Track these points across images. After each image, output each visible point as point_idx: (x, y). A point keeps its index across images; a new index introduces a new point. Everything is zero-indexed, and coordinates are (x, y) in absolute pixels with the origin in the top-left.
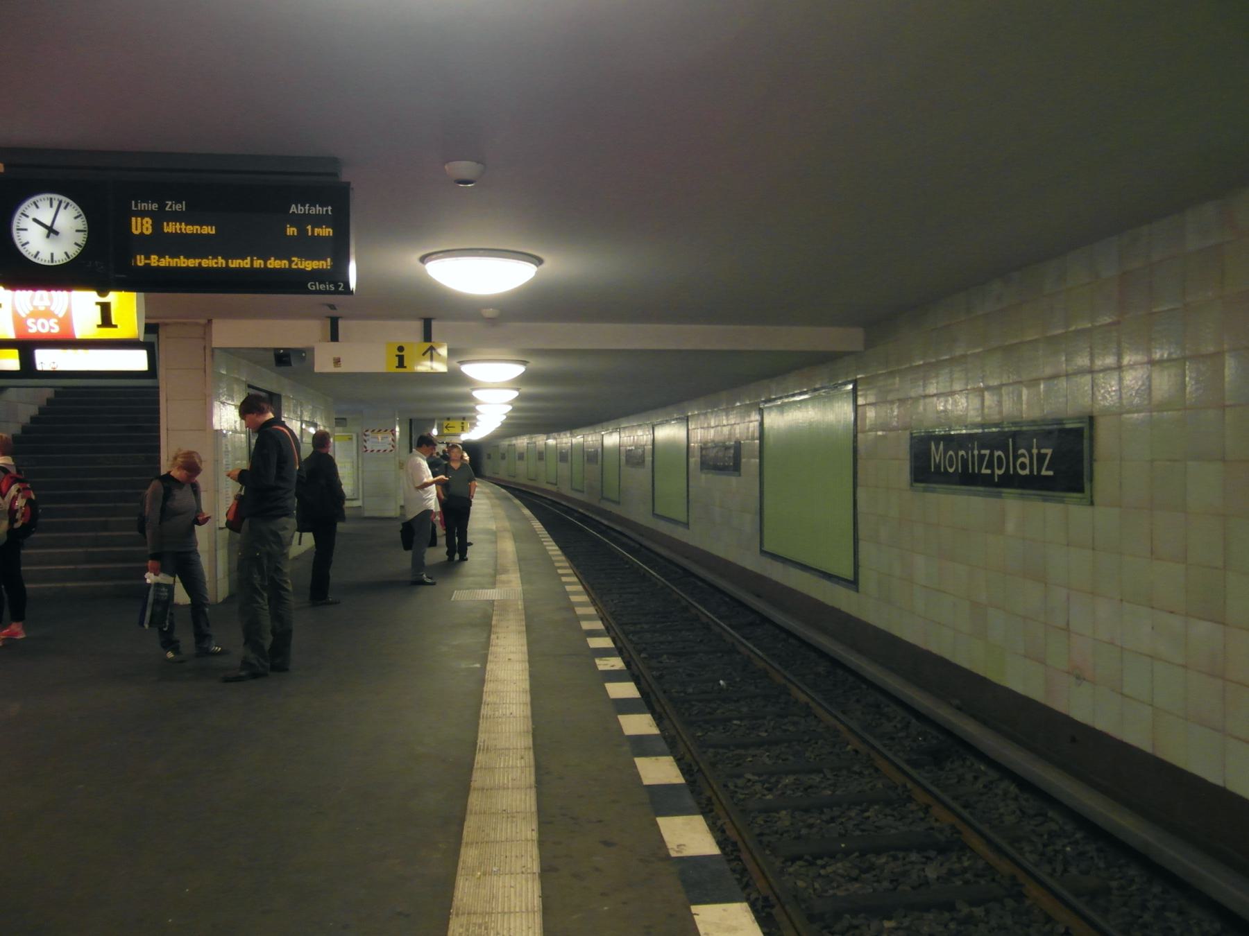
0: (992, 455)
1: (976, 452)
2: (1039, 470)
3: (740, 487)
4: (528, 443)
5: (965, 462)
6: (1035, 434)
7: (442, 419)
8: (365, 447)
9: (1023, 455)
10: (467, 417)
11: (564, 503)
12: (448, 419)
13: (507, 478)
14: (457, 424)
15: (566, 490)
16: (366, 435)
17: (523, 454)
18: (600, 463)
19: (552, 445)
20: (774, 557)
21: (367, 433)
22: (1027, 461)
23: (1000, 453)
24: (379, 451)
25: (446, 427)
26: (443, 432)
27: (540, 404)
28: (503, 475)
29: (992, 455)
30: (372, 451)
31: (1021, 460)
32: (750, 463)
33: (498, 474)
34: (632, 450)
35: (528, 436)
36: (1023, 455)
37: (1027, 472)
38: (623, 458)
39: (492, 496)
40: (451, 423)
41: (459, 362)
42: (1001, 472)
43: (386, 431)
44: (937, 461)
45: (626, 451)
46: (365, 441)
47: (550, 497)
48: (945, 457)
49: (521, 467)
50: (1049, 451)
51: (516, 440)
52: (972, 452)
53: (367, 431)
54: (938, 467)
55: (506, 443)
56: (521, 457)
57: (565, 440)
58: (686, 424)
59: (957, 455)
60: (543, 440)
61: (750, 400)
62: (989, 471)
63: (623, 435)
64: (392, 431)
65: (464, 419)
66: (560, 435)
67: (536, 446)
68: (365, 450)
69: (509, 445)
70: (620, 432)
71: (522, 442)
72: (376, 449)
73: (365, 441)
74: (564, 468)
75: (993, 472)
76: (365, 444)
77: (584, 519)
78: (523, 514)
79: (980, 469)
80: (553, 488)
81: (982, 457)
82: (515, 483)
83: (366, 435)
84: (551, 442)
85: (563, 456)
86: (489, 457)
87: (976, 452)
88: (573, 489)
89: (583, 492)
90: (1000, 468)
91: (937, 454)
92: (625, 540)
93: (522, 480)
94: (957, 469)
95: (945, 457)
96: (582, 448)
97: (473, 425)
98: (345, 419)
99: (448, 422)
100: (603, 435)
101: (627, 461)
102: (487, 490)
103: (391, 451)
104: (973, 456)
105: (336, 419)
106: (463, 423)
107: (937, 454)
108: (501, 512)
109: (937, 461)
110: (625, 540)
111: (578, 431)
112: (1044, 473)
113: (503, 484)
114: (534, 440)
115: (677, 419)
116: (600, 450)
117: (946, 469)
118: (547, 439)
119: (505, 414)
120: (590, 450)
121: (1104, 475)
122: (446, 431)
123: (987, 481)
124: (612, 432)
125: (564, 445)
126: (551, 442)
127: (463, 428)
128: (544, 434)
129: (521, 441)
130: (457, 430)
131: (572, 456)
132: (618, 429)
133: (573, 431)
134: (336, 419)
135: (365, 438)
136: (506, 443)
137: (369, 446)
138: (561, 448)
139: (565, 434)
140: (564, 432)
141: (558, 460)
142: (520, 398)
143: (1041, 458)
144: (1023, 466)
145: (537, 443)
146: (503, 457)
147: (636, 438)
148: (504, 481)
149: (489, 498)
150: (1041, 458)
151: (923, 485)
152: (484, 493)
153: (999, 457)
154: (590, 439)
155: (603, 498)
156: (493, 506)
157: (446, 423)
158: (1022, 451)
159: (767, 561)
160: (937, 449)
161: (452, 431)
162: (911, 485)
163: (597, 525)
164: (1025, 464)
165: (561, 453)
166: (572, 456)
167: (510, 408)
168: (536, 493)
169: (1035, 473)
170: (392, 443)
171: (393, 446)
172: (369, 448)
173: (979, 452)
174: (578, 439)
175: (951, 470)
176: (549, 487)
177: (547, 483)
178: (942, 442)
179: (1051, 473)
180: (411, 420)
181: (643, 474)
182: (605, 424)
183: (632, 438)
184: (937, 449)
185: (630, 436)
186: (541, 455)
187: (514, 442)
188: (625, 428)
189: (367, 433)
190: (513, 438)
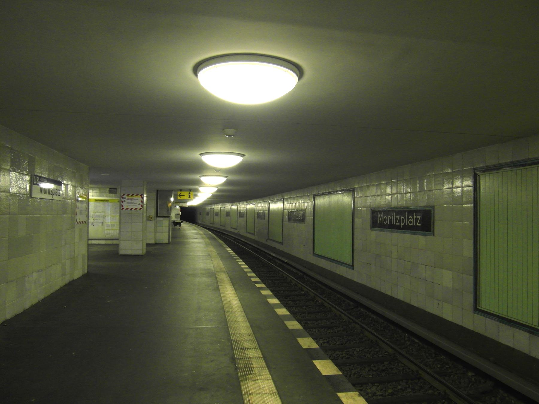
0: (400, 218)
1: (395, 217)
2: (416, 223)
3: (304, 228)
4: (221, 208)
5: (390, 220)
6: (383, 211)
7: (176, 190)
8: (122, 206)
9: (411, 218)
10: (193, 192)
11: (242, 240)
12: (181, 190)
13: (209, 225)
14: (186, 194)
15: (242, 232)
16: (123, 198)
17: (218, 213)
18: (245, 217)
19: (235, 209)
20: (319, 256)
21: (124, 197)
22: (412, 221)
23: (403, 217)
24: (132, 209)
25: (179, 195)
26: (177, 198)
27: (224, 194)
28: (207, 223)
29: (400, 218)
30: (127, 209)
31: (410, 220)
32: (309, 218)
33: (205, 222)
34: (294, 211)
35: (221, 204)
36: (411, 218)
37: (412, 224)
38: (256, 215)
39: (204, 236)
40: (182, 193)
41: (200, 176)
42: (403, 224)
43: (137, 195)
44: (380, 219)
45: (289, 213)
46: (122, 202)
47: (233, 236)
48: (383, 218)
49: (217, 219)
50: (420, 217)
51: (215, 205)
52: (393, 217)
53: (124, 195)
54: (380, 221)
55: (209, 207)
56: (217, 214)
57: (243, 206)
58: (352, 193)
59: (388, 218)
60: (229, 206)
61: (367, 184)
62: (399, 224)
63: (285, 203)
64: (141, 195)
65: (190, 190)
66: (239, 203)
67: (225, 209)
68: (122, 208)
69: (211, 208)
70: (283, 201)
71: (218, 207)
72: (130, 207)
73: (122, 202)
74: (241, 221)
75: (400, 224)
76: (122, 203)
77: (256, 250)
78: (219, 242)
79: (396, 223)
80: (236, 231)
81: (396, 219)
82: (224, 230)
83: (123, 198)
84: (234, 207)
85: (241, 214)
86: (200, 214)
87: (395, 217)
88: (247, 232)
89: (254, 234)
90: (403, 223)
91: (380, 217)
92: (289, 268)
93: (217, 226)
94: (388, 222)
95: (383, 218)
96: (254, 211)
97: (195, 196)
98: (116, 189)
99: (181, 192)
100: (269, 203)
101: (290, 219)
102: (201, 232)
103: (140, 209)
104: (393, 218)
105: (110, 189)
106: (190, 193)
107: (381, 217)
108: (213, 250)
109: (380, 219)
110: (289, 268)
111: (251, 201)
112: (418, 225)
113: (207, 227)
114: (224, 206)
115: (340, 191)
116: (267, 211)
117: (408, 224)
118: (232, 206)
119: (212, 193)
120: (260, 211)
121: (438, 226)
122: (179, 198)
123: (398, 228)
124: (277, 201)
125: (242, 209)
126: (234, 207)
127: (190, 197)
128: (230, 203)
129: (217, 207)
130: (186, 197)
131: (247, 214)
132: (283, 200)
133: (248, 201)
134: (110, 189)
135: (122, 199)
136: (209, 207)
137: (125, 206)
138: (240, 210)
139: (243, 203)
140: (242, 202)
141: (226, 216)
142: (227, 183)
143: (417, 219)
144: (411, 222)
145: (226, 207)
146: (208, 214)
147: (297, 204)
148: (207, 226)
149: (203, 238)
150: (417, 219)
151: (380, 229)
152: (200, 234)
153: (403, 219)
154: (259, 205)
155: (268, 239)
156: (207, 245)
157: (179, 193)
158: (410, 217)
159: (315, 258)
160: (380, 215)
161: (183, 198)
162: (371, 228)
163: (265, 255)
164: (411, 221)
165: (240, 213)
166: (247, 214)
167: (216, 189)
168: (225, 233)
169: (415, 225)
170: (141, 204)
171: (142, 206)
172: (125, 207)
173: (416, 217)
174: (251, 206)
175: (385, 223)
176: (232, 230)
177: (232, 228)
178: (379, 213)
179: (420, 225)
180: (157, 191)
181: (304, 228)
182: (271, 197)
183: (294, 204)
184: (380, 215)
185: (292, 204)
186: (228, 214)
187: (213, 207)
188: (287, 199)
189: (124, 197)
190: (213, 205)
